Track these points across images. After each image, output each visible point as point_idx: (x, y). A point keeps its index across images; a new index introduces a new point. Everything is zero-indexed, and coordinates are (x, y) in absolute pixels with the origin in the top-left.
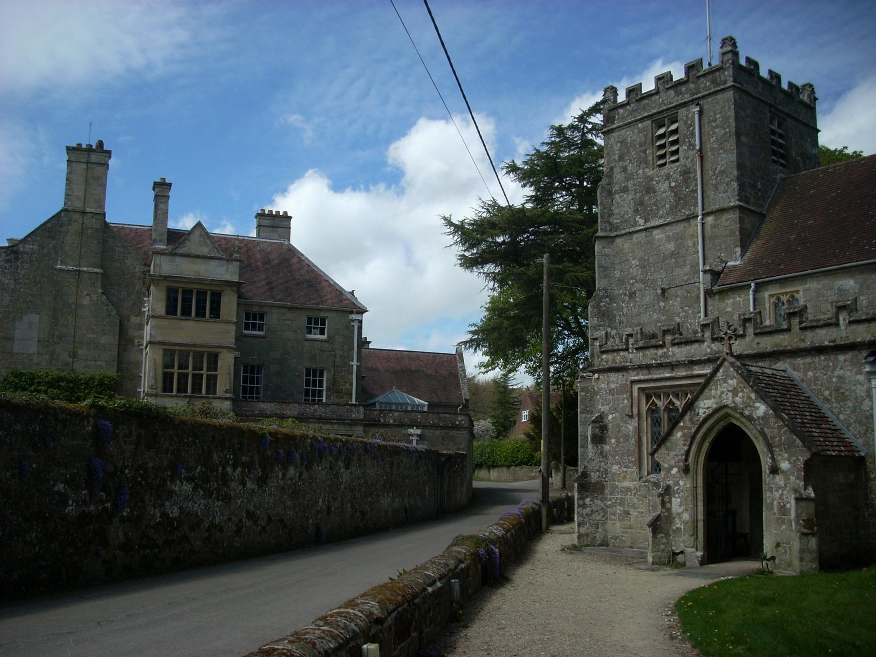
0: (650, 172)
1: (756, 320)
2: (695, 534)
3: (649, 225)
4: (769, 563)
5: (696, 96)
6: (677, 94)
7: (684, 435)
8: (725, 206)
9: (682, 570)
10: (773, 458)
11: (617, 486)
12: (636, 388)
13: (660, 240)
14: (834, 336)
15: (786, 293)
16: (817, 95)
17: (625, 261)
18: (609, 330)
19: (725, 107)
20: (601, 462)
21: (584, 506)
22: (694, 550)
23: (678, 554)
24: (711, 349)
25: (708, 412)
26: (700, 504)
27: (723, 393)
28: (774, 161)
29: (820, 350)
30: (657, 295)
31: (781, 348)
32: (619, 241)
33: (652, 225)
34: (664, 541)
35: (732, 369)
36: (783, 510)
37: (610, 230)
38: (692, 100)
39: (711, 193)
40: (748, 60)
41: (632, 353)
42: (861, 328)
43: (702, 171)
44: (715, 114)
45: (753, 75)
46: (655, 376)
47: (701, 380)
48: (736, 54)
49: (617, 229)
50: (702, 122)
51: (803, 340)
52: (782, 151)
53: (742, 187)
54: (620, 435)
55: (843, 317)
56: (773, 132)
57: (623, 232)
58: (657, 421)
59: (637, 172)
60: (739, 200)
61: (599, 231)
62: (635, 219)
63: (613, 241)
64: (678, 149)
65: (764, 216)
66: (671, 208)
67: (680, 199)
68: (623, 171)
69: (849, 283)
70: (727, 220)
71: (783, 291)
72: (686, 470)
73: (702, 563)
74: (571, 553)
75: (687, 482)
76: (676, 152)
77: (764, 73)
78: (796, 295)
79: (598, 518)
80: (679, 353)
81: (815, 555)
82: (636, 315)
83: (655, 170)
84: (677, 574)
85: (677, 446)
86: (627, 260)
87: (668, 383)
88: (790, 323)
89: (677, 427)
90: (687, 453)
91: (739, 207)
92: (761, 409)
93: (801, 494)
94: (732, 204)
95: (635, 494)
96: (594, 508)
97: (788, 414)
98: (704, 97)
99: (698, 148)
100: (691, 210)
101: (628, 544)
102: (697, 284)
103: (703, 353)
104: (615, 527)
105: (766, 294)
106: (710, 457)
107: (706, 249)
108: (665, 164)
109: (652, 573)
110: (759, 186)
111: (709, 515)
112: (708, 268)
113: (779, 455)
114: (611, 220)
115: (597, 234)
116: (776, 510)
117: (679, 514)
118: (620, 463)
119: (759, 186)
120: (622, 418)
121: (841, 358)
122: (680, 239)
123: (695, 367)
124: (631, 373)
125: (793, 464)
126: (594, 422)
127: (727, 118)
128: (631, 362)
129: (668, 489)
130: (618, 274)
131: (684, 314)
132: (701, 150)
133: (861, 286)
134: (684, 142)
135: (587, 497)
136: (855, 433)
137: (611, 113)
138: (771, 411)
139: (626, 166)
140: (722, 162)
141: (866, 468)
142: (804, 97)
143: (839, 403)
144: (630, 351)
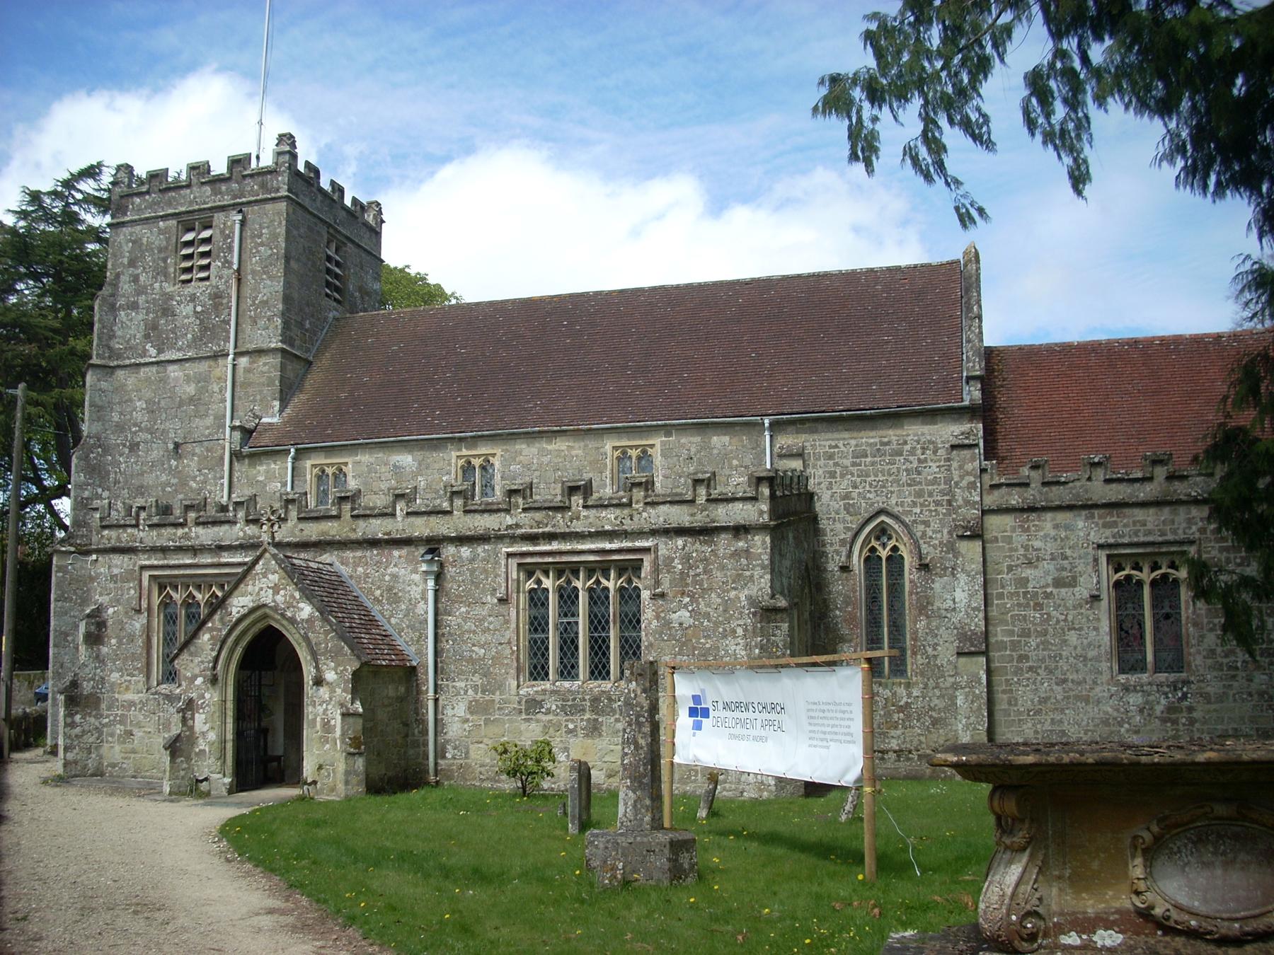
0: (169, 288)
1: (300, 502)
2: (222, 757)
3: (162, 357)
4: (310, 788)
5: (238, 200)
6: (215, 193)
7: (212, 638)
8: (264, 346)
9: (207, 800)
10: (317, 667)
11: (117, 700)
12: (146, 575)
13: (176, 379)
14: (390, 528)
15: (333, 465)
16: (384, 217)
17: (127, 401)
18: (100, 490)
19: (274, 221)
20: (96, 668)
21: (72, 725)
22: (220, 776)
23: (202, 781)
24: (245, 532)
25: (243, 611)
26: (230, 721)
27: (261, 589)
28: (327, 295)
29: (373, 543)
30: (167, 450)
31: (328, 538)
32: (120, 374)
33: (167, 358)
34: (185, 765)
35: (273, 562)
36: (327, 727)
37: (110, 357)
38: (234, 205)
39: (247, 327)
41: (143, 531)
42: (419, 521)
43: (238, 297)
44: (261, 228)
45: (312, 185)
46: (172, 562)
47: (240, 570)
48: (294, 156)
49: (119, 357)
50: (244, 234)
51: (354, 530)
52: (338, 283)
53: (286, 325)
55: (400, 507)
56: (329, 259)
57: (127, 362)
58: (171, 617)
59: (152, 285)
60: (281, 341)
61: (94, 357)
62: (144, 347)
63: (112, 373)
64: (210, 264)
65: (310, 363)
66: (194, 339)
67: (206, 329)
68: (133, 281)
69: (406, 460)
70: (265, 364)
71: (329, 461)
72: (214, 680)
73: (230, 792)
74: (57, 786)
75: (215, 695)
76: (207, 267)
77: (325, 184)
78: (343, 467)
79: (91, 740)
80: (205, 535)
81: (362, 777)
82: (138, 474)
83: (177, 287)
84: (205, 805)
85: (203, 650)
86: (131, 400)
88: (340, 509)
89: (204, 629)
90: (216, 659)
91: (283, 351)
92: (306, 610)
93: (348, 709)
94: (273, 345)
95: (141, 709)
96: (86, 728)
97: (336, 617)
98: (249, 203)
99: (235, 267)
100: (219, 346)
101: (131, 772)
102: (221, 442)
103: (234, 537)
104: (113, 752)
105: (308, 463)
106: (244, 664)
107: (236, 398)
108: (190, 281)
109: (171, 804)
110: (308, 326)
111: (239, 734)
112: (237, 423)
113: (325, 664)
115: (91, 362)
117: (203, 733)
118: (121, 670)
119: (308, 326)
120: (126, 613)
121: (396, 553)
122: (203, 380)
123: (223, 554)
125: (340, 674)
126: (88, 616)
127: (275, 236)
128: (141, 542)
129: (190, 702)
130: (116, 417)
131: (202, 478)
132: (239, 271)
133: (420, 465)
134: (218, 256)
135: (76, 713)
136: (407, 639)
137: (123, 201)
138: (317, 614)
140: (265, 291)
141: (417, 680)
142: (369, 217)
143: (391, 605)
144: (141, 527)
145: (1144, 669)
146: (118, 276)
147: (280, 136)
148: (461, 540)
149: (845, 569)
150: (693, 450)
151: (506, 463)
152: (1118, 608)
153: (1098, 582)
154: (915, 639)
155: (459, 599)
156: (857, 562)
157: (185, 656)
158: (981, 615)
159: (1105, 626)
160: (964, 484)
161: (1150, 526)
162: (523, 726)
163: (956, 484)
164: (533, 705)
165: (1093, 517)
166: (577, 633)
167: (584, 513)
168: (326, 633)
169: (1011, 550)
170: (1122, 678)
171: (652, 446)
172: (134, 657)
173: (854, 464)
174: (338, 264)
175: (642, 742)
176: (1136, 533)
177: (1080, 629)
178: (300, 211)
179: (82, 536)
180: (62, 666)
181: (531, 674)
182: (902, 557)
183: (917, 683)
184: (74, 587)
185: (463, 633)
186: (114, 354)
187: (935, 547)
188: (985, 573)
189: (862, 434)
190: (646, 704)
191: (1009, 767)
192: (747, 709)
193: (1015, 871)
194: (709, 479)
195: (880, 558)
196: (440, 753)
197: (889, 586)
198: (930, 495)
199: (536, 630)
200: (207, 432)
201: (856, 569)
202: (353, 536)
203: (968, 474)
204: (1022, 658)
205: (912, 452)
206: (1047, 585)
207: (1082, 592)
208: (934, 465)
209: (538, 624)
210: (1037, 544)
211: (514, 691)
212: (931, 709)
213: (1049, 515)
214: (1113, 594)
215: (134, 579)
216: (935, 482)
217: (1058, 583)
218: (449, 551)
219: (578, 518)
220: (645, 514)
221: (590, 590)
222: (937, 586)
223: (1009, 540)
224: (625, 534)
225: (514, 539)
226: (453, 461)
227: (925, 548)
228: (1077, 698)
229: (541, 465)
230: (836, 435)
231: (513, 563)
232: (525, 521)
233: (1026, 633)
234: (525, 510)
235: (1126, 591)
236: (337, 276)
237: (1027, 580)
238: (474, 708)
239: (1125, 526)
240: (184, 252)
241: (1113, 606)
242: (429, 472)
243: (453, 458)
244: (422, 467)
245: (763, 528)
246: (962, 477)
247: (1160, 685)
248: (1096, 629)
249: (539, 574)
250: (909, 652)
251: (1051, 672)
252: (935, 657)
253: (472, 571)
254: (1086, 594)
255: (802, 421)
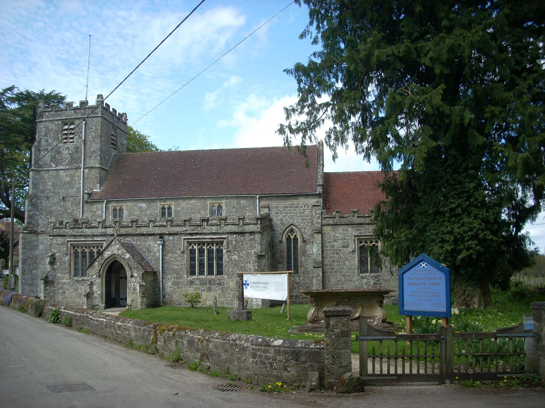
2: (102, 298)
3: (57, 168)
5: (84, 116)
6: (75, 113)
7: (98, 264)
8: (94, 166)
10: (131, 272)
12: (69, 243)
13: (63, 175)
14: (148, 230)
16: (127, 118)
18: (36, 212)
31: (129, 233)
32: (42, 173)
33: (59, 168)
36: (135, 289)
37: (38, 167)
38: (82, 118)
39: (88, 160)
40: (113, 109)
42: (157, 228)
44: (92, 126)
46: (78, 240)
49: (41, 167)
54: (61, 262)
56: (112, 135)
57: (45, 169)
64: (74, 137)
66: (69, 162)
67: (73, 159)
70: (94, 172)
71: (117, 205)
72: (99, 276)
76: (73, 138)
79: (52, 294)
80: (88, 231)
86: (46, 182)
87: (83, 243)
91: (100, 168)
92: (128, 256)
94: (97, 166)
96: (50, 291)
99: (83, 139)
105: (110, 205)
106: (107, 272)
108: (67, 142)
114: (39, 162)
116: (132, 289)
117: (96, 292)
121: (150, 238)
122: (72, 176)
124: (67, 237)
125: (138, 274)
127: (97, 129)
130: (41, 188)
132: (84, 140)
133: (148, 207)
137: (42, 113)
139: (48, 139)
145: (367, 272)
146: (40, 139)
147: (98, 95)
148: (170, 234)
149: (281, 242)
150: (235, 204)
151: (175, 206)
152: (361, 254)
153: (355, 247)
154: (301, 263)
155: (169, 252)
156: (284, 239)
157: (90, 269)
158: (321, 256)
159: (356, 259)
160: (316, 217)
161: (370, 230)
162: (189, 289)
163: (314, 217)
164: (192, 283)
165: (354, 227)
166: (204, 262)
167: (207, 227)
168: (134, 262)
169: (330, 237)
170: (361, 275)
171: (222, 203)
172: (65, 269)
173: (284, 210)
174: (114, 136)
175: (240, 291)
176: (366, 232)
177: (349, 260)
178: (104, 120)
179: (30, 227)
180: (24, 271)
181: (191, 274)
182: (298, 238)
183: (301, 276)
184: (28, 244)
185: (171, 262)
186: (41, 166)
187: (307, 235)
188: (322, 243)
189: (286, 201)
190: (241, 282)
191: (312, 292)
192: (259, 283)
193: (313, 310)
194: (243, 218)
195: (291, 238)
196: (164, 297)
197: (293, 247)
198: (306, 220)
199: (192, 261)
200: (74, 194)
201: (284, 241)
202: (136, 233)
203: (318, 214)
204: (332, 269)
205: (301, 207)
206: (340, 247)
207: (350, 249)
208: (307, 211)
209: (192, 259)
210: (337, 235)
211: (186, 279)
212: (306, 283)
213: (341, 227)
214: (359, 250)
215: (65, 245)
216: (308, 216)
217: (343, 247)
218: (166, 237)
219: (205, 229)
220: (224, 228)
221: (208, 249)
222: (308, 247)
223: (329, 234)
224: (219, 234)
225: (186, 234)
226: (159, 206)
227: (304, 236)
228: (349, 280)
229: (187, 208)
230: (278, 201)
231: (186, 241)
232: (189, 229)
233: (334, 261)
234: (189, 226)
235: (362, 249)
236: (114, 140)
237: (334, 246)
238: (174, 284)
239: (363, 230)
240: (64, 132)
241: (359, 253)
242: (151, 209)
243: (159, 205)
244: (149, 208)
245: (259, 232)
246: (316, 215)
247: (372, 277)
248: (354, 260)
249: (193, 245)
250: (299, 267)
251: (341, 273)
252: (307, 268)
253: (173, 244)
254: (351, 250)
255: (268, 197)
